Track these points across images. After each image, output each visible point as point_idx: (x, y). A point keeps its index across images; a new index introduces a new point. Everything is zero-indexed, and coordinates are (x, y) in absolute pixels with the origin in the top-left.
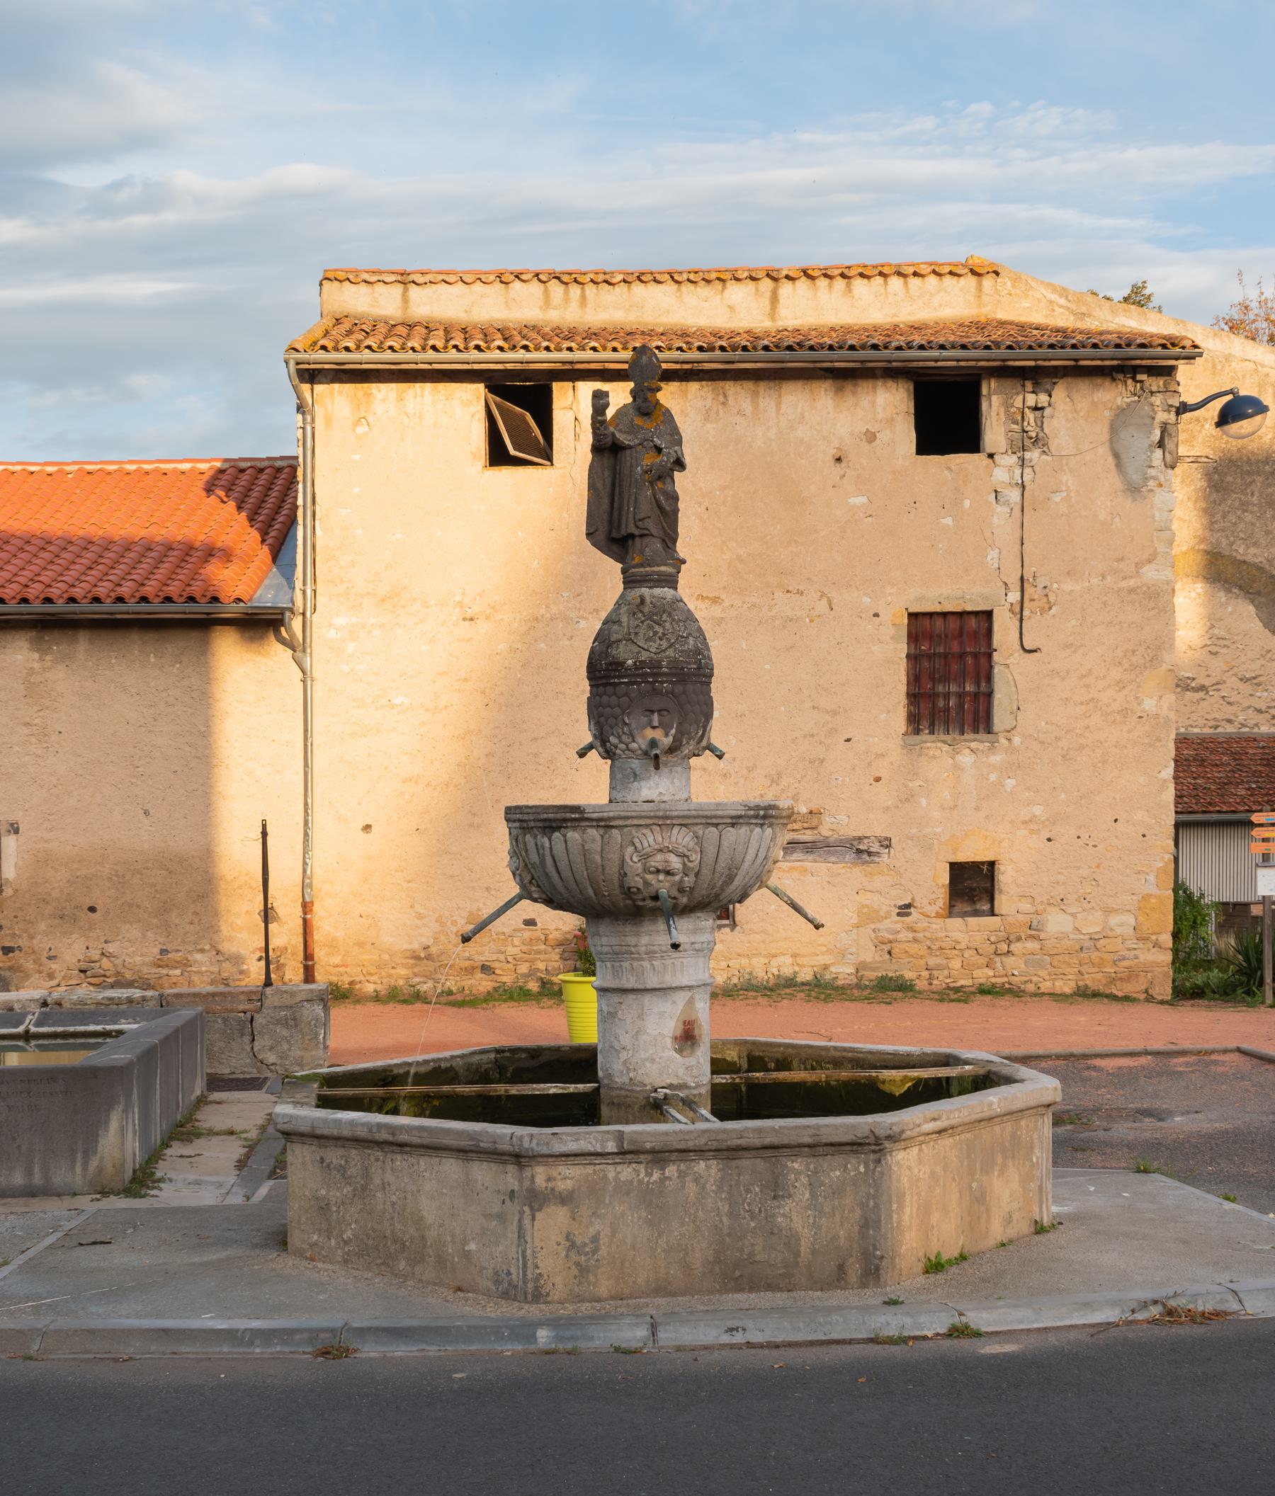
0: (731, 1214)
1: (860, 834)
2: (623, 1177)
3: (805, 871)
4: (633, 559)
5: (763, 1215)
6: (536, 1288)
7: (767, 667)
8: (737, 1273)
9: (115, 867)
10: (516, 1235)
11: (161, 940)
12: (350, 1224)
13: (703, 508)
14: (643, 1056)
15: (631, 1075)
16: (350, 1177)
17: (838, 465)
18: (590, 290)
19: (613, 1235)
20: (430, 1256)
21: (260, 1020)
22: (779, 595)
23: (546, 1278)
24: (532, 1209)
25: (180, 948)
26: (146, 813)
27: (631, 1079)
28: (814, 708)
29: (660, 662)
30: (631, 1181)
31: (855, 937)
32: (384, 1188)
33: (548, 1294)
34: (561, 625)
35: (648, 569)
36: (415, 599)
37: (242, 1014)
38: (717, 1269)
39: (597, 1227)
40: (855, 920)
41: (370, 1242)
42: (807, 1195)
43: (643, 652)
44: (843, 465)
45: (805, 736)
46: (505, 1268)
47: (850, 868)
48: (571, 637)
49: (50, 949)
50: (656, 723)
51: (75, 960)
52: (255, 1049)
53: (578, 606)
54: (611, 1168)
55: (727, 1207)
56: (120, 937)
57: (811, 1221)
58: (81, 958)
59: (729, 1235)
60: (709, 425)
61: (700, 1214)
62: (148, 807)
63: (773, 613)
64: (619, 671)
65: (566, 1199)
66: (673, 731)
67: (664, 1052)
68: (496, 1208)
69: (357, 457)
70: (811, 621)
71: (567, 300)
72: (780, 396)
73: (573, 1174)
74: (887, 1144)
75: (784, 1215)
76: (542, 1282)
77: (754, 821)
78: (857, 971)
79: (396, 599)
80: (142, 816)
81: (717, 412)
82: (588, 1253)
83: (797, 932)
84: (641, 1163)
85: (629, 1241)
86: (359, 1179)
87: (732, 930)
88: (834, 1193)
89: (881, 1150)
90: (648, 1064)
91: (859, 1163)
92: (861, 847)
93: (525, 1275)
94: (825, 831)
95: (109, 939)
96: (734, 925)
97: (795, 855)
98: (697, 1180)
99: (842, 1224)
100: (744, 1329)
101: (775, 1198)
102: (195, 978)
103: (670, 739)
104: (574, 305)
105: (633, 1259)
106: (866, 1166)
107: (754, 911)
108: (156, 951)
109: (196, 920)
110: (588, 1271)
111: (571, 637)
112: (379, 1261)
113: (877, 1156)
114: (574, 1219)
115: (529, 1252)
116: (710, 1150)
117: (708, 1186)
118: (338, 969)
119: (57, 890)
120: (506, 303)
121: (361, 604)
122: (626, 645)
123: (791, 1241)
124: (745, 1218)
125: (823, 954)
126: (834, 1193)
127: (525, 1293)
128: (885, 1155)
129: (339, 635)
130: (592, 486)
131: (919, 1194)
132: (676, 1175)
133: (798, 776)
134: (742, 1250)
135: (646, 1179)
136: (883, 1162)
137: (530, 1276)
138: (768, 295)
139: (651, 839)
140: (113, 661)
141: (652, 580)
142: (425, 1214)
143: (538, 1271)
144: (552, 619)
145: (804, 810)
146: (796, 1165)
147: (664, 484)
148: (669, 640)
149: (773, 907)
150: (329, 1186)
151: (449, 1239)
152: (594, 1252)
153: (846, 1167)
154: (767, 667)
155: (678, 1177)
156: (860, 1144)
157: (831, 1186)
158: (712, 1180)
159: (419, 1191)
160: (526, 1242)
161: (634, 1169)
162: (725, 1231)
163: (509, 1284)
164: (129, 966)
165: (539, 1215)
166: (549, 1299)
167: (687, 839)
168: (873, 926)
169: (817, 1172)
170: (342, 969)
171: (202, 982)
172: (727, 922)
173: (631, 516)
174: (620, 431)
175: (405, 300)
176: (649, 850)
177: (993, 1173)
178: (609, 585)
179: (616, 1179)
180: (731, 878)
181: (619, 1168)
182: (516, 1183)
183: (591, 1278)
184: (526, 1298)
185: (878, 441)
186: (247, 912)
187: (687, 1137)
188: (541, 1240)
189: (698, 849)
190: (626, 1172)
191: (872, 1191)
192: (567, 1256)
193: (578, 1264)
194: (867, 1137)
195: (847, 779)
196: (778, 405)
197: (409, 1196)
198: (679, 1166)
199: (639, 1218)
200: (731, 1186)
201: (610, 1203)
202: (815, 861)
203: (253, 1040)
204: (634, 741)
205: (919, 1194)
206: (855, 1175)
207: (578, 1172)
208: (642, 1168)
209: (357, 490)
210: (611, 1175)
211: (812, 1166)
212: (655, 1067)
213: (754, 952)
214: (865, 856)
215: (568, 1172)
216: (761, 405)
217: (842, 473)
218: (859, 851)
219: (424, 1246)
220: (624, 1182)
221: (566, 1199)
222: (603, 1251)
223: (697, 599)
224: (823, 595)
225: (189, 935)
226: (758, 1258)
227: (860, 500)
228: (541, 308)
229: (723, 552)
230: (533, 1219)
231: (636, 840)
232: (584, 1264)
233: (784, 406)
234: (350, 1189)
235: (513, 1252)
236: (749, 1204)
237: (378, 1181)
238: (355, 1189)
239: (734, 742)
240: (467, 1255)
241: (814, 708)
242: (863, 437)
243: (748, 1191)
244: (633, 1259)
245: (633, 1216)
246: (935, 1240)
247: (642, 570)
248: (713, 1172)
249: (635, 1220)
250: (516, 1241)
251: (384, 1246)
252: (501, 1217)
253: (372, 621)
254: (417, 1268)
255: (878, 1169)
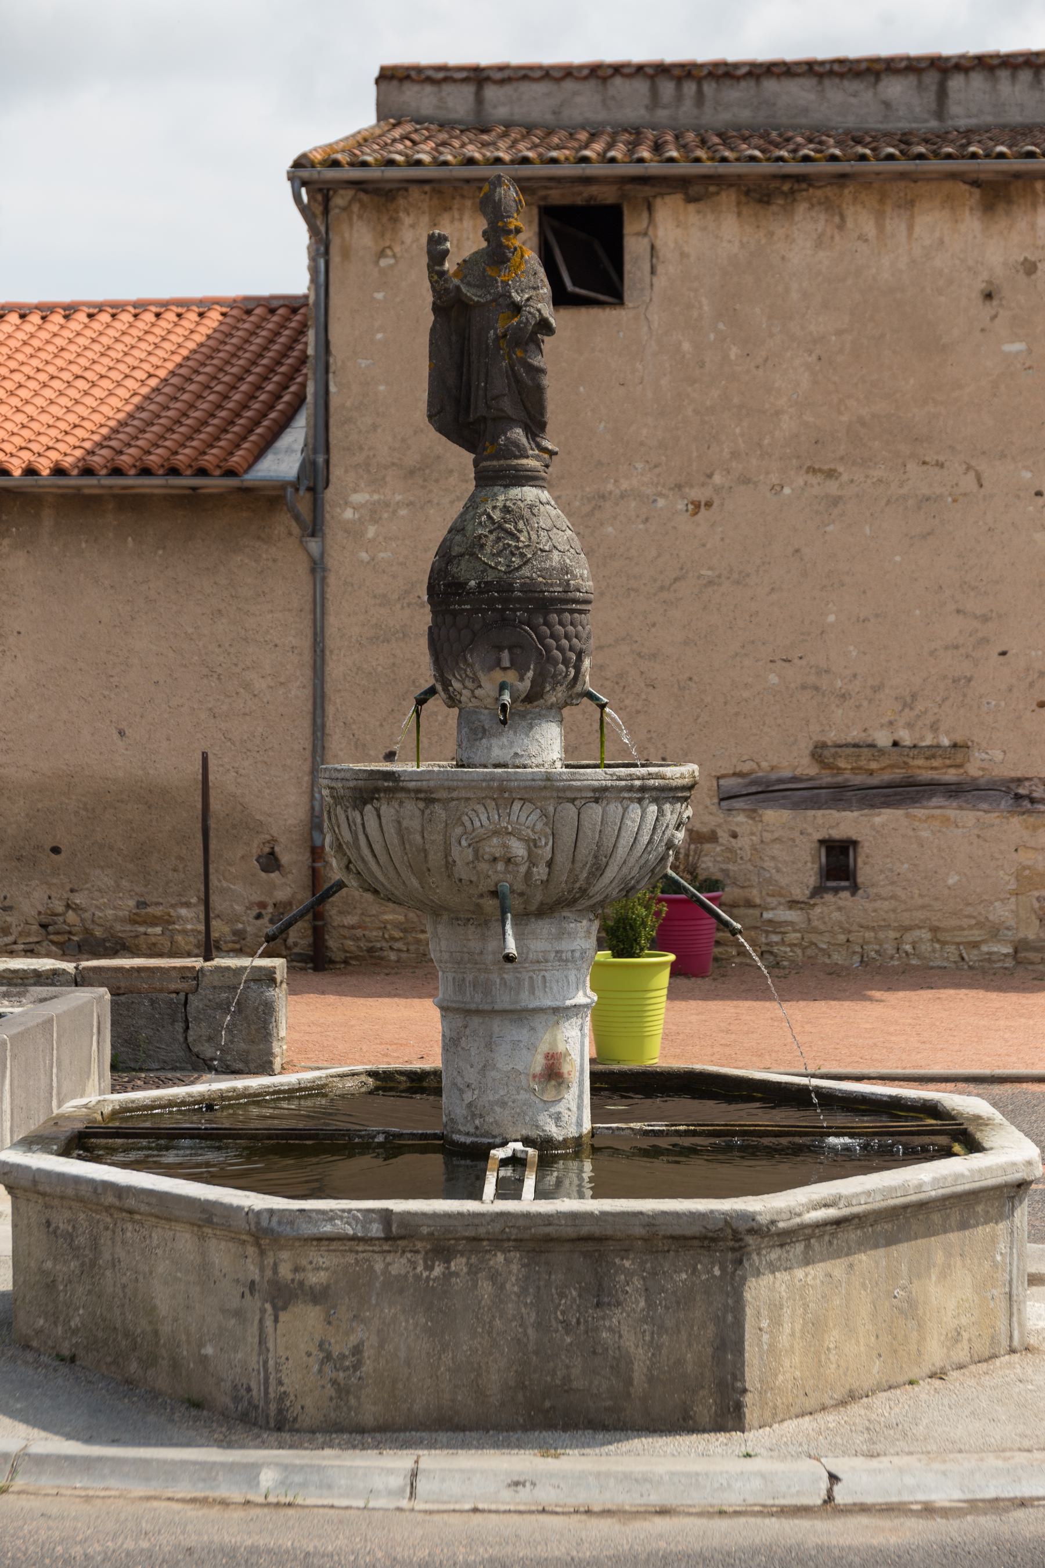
0: (538, 1325)
1: (1019, 774)
2: (394, 1270)
3: (946, 820)
4: (485, 449)
5: (582, 1327)
6: (280, 1411)
7: (898, 558)
8: (547, 1404)
9: (83, 799)
10: (256, 1340)
11: (138, 890)
12: (77, 1309)
13: (814, 357)
14: (491, 1098)
15: (477, 1122)
16: (78, 1248)
17: (988, 303)
18: (709, 88)
19: (381, 1346)
20: (163, 1359)
21: (195, 1001)
22: (911, 466)
23: (292, 1398)
24: (275, 1307)
25: (161, 900)
26: (121, 733)
27: (477, 1128)
28: (958, 611)
29: (511, 584)
30: (406, 1275)
31: (1013, 907)
32: (114, 1266)
33: (295, 1420)
34: (633, 504)
35: (502, 462)
36: (451, 471)
37: (174, 995)
38: (520, 1397)
39: (360, 1334)
40: (1013, 886)
41: (100, 1334)
42: (642, 1304)
43: (490, 571)
44: (995, 303)
45: (947, 648)
46: (245, 1381)
47: (1007, 818)
48: (647, 519)
49: (5, 898)
50: (506, 663)
51: (34, 913)
52: (190, 1039)
53: (655, 480)
54: (378, 1257)
55: (533, 1315)
56: (88, 885)
57: (648, 1338)
58: (41, 909)
59: (536, 1353)
60: (821, 254)
61: (498, 1322)
62: (123, 725)
63: (904, 491)
64: (460, 595)
65: (318, 1296)
66: (530, 674)
67: (518, 1094)
68: (235, 1303)
69: (379, 296)
70: (955, 501)
71: (679, 98)
72: (912, 217)
73: (328, 1263)
74: (750, 1240)
75: (610, 1329)
76: (288, 1404)
77: (626, 795)
78: (1016, 951)
79: (427, 471)
80: (116, 736)
81: (832, 237)
82: (348, 1368)
83: (937, 899)
84: (417, 1252)
85: (402, 1355)
86: (87, 1252)
87: (853, 894)
88: (678, 1303)
89: (741, 1248)
90: (497, 1109)
91: (713, 1265)
92: (1022, 791)
93: (266, 1393)
94: (973, 770)
95: (76, 887)
96: (854, 889)
97: (934, 800)
98: (493, 1278)
99: (690, 1345)
100: (533, 1484)
101: (598, 1305)
102: (179, 938)
103: (527, 683)
104: (688, 105)
105: (408, 1379)
106: (723, 1269)
107: (882, 871)
108: (132, 903)
109: (181, 866)
110: (348, 1392)
111: (647, 519)
112: (109, 1359)
113: (738, 1254)
114: (329, 1323)
115: (271, 1363)
116: (509, 1240)
117: (508, 1286)
118: (354, 931)
119: (14, 826)
120: (604, 102)
121: (384, 478)
122: (469, 561)
123: (621, 1366)
124: (557, 1331)
125: (971, 927)
126: (678, 1303)
127: (267, 1416)
128: (749, 1254)
129: (357, 516)
130: (434, 353)
131: (806, 1306)
132: (465, 1270)
133: (938, 699)
134: (554, 1373)
135: (425, 1274)
136: (746, 1264)
137: (272, 1395)
138: (934, 88)
139: (484, 817)
140: (84, 545)
141: (508, 477)
142: (158, 1302)
143: (282, 1389)
144: (622, 497)
145: (946, 742)
146: (627, 1264)
147: (526, 351)
148: (522, 555)
149: (906, 866)
150: (55, 1259)
151: (184, 1337)
152: (356, 1367)
153: (695, 1269)
154: (898, 558)
155: (468, 1273)
156: (713, 1240)
157: (674, 1293)
158: (513, 1279)
159: (151, 1273)
160: (268, 1350)
161: (409, 1260)
162: (531, 1347)
163: (250, 1403)
164: (101, 921)
165: (283, 1316)
166: (297, 1426)
167: (534, 817)
168: (1036, 894)
169: (656, 1274)
170: (359, 932)
171: (187, 943)
172: (844, 884)
173: (481, 393)
174: (469, 284)
175: (479, 100)
176: (482, 831)
177: (930, 1278)
178: (695, 454)
179: (386, 1271)
180: (598, 870)
181: (389, 1258)
182: (257, 1271)
183: (353, 1401)
184: (268, 1423)
185: (1039, 273)
186: (243, 857)
187: (476, 1221)
188: (287, 1348)
189: (549, 831)
190: (399, 1265)
191: (730, 1301)
192: (320, 1371)
193: (334, 1382)
194: (721, 1230)
195: (1003, 704)
196: (910, 228)
197: (141, 1278)
198: (469, 1259)
199: (416, 1325)
200: (539, 1288)
201: (377, 1304)
202: (961, 808)
203: (187, 1028)
204: (480, 686)
205: (806, 1306)
206: (707, 1280)
207: (335, 1261)
208: (420, 1259)
209: (379, 336)
210: (379, 1267)
211: (648, 1265)
212: (507, 1112)
213: (883, 923)
214: (1026, 804)
215: (321, 1260)
216: (889, 228)
217: (993, 312)
218: (1018, 797)
219: (157, 1343)
220: (396, 1277)
221: (318, 1296)
222: (368, 1366)
223: (807, 472)
224: (969, 468)
225: (171, 884)
226: (575, 1385)
227: (1018, 347)
228: (647, 107)
229: (840, 413)
230: (276, 1320)
231: (465, 818)
232: (342, 1382)
233: (917, 230)
234: (77, 1263)
235: (254, 1361)
236: (563, 1313)
237: (107, 1256)
238: (83, 1264)
239: (854, 654)
240: (204, 1360)
241: (958, 611)
242: (1019, 267)
243: (562, 1295)
244: (408, 1379)
245: (407, 1321)
246: (833, 1366)
247: (495, 463)
248: (514, 1268)
249: (411, 1327)
250: (256, 1347)
251: (114, 1340)
252: (238, 1314)
253: (398, 497)
254: (149, 1373)
255: (739, 1272)
